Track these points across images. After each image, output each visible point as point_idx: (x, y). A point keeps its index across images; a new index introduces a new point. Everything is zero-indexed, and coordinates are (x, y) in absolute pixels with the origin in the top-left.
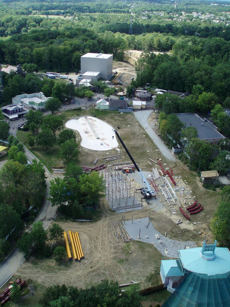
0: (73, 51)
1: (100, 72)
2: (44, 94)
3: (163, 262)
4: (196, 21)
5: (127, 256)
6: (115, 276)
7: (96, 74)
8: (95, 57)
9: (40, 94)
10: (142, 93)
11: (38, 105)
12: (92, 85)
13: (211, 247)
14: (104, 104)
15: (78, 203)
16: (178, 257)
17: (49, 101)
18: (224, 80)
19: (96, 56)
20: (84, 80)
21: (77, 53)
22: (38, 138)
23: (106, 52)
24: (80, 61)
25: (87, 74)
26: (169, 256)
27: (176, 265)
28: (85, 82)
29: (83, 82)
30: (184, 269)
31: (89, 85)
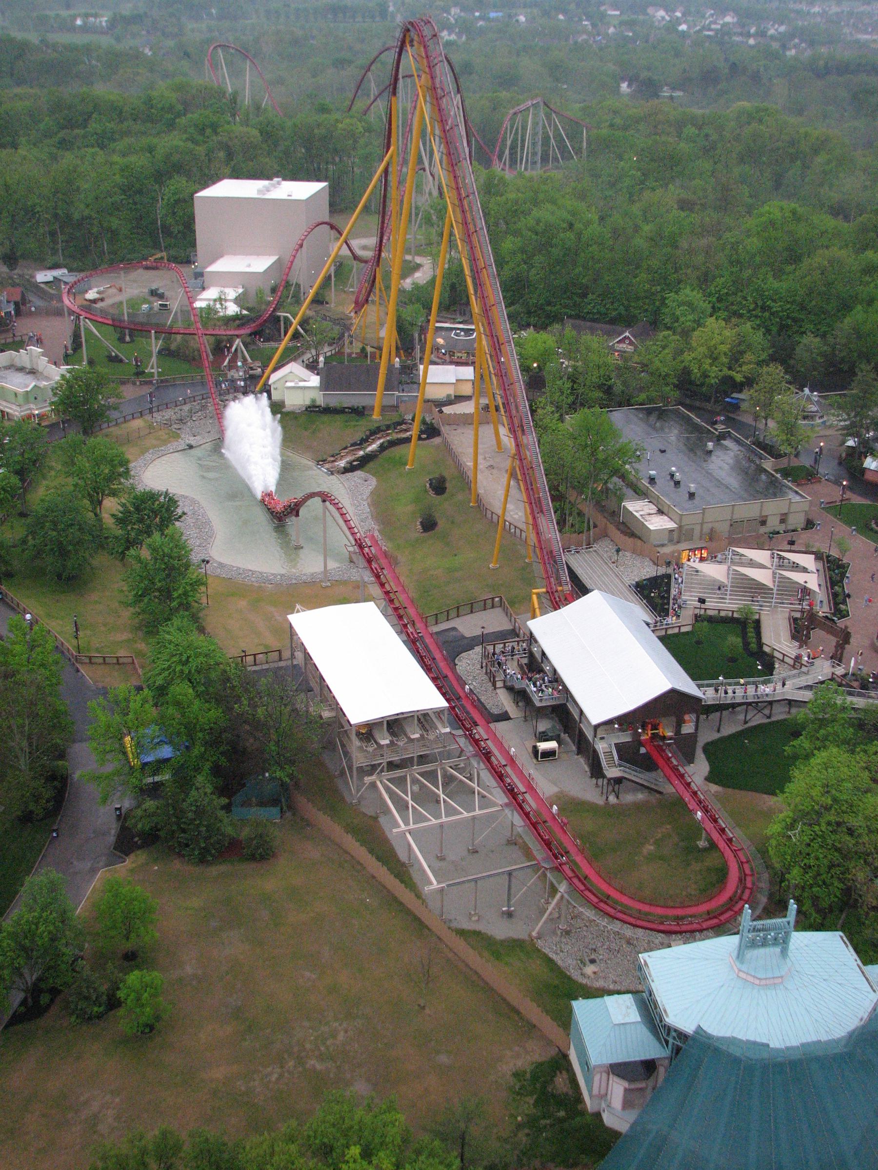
0: (160, 177)
1: (277, 257)
2: (43, 355)
3: (580, 1007)
4: (495, 688)
5: (598, 394)
6: (530, 489)
7: (260, 264)
8: (254, 195)
9: (30, 354)
10: (456, 335)
11: (21, 400)
12: (245, 312)
13: (774, 929)
14: (302, 384)
15: (209, 791)
16: (640, 988)
17: (68, 381)
18: (790, 268)
19: (259, 191)
20: (211, 293)
21: (179, 182)
22: (27, 536)
23: (295, 176)
24: (193, 214)
25: (222, 266)
26: (600, 984)
27: (634, 1016)
28: (215, 300)
29: (209, 300)
30: (669, 1029)
31: (232, 309)
